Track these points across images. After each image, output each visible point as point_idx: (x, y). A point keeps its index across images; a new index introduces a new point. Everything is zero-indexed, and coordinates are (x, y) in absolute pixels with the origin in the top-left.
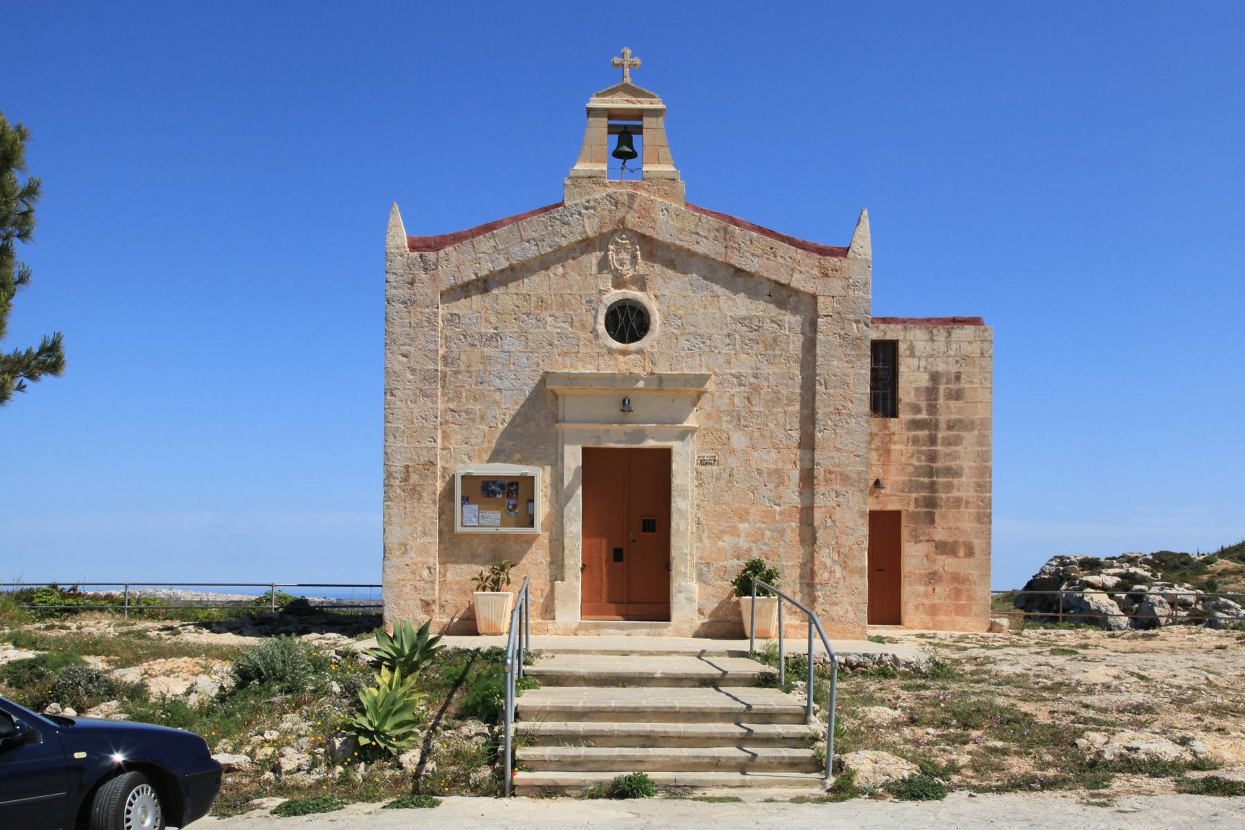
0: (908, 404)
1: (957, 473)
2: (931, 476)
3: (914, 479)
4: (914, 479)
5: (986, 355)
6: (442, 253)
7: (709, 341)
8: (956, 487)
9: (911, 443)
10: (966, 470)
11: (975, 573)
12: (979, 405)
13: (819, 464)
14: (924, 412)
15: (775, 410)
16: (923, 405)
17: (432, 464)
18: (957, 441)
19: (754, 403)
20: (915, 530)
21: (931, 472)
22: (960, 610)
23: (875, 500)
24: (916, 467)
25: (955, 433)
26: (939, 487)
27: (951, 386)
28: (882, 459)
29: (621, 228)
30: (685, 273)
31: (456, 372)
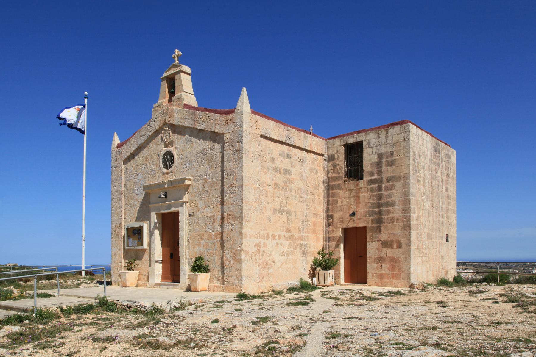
0: (368, 172)
1: (392, 204)
2: (379, 207)
3: (371, 210)
4: (371, 210)
5: (406, 139)
6: (123, 147)
7: (191, 163)
8: (392, 212)
9: (369, 191)
10: (397, 203)
11: (402, 257)
12: (403, 167)
13: (225, 211)
14: (376, 175)
15: (212, 189)
16: (375, 171)
17: (121, 224)
18: (392, 187)
19: (205, 187)
20: (372, 235)
21: (379, 205)
22: (395, 276)
23: (353, 222)
24: (372, 203)
25: (391, 183)
26: (383, 213)
27: (388, 159)
28: (356, 201)
29: (165, 124)
30: (184, 136)
31: (128, 190)
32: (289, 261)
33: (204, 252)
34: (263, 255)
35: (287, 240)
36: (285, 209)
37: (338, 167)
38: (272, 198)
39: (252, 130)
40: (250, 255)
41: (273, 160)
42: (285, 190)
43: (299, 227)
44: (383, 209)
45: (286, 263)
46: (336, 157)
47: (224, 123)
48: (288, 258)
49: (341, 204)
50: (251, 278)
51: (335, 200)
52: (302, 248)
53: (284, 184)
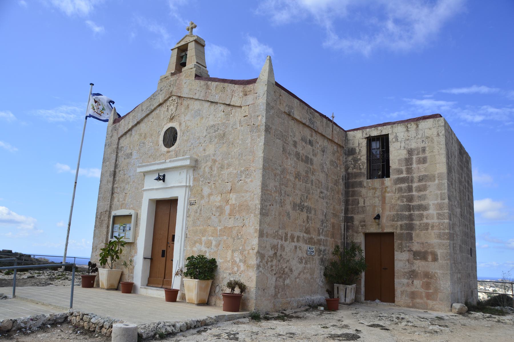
1: (425, 208)
2: (410, 211)
5: (440, 135)
6: (120, 122)
10: (431, 207)
14: (404, 172)
16: (404, 168)
21: (409, 208)
25: (424, 183)
32: (307, 270)
33: (206, 252)
34: (279, 261)
35: (306, 244)
36: (306, 204)
37: (359, 162)
38: (293, 190)
39: (276, 104)
40: (266, 260)
41: (295, 144)
42: (306, 182)
43: (318, 228)
44: (414, 213)
45: (304, 273)
46: (357, 151)
47: (241, 94)
48: (307, 266)
49: (363, 205)
50: (265, 291)
51: (356, 199)
52: (321, 254)
53: (305, 174)
